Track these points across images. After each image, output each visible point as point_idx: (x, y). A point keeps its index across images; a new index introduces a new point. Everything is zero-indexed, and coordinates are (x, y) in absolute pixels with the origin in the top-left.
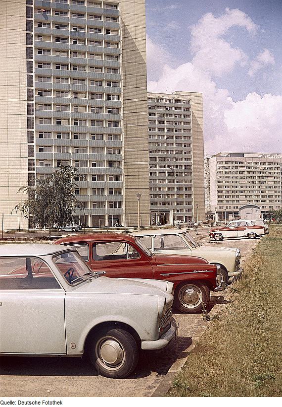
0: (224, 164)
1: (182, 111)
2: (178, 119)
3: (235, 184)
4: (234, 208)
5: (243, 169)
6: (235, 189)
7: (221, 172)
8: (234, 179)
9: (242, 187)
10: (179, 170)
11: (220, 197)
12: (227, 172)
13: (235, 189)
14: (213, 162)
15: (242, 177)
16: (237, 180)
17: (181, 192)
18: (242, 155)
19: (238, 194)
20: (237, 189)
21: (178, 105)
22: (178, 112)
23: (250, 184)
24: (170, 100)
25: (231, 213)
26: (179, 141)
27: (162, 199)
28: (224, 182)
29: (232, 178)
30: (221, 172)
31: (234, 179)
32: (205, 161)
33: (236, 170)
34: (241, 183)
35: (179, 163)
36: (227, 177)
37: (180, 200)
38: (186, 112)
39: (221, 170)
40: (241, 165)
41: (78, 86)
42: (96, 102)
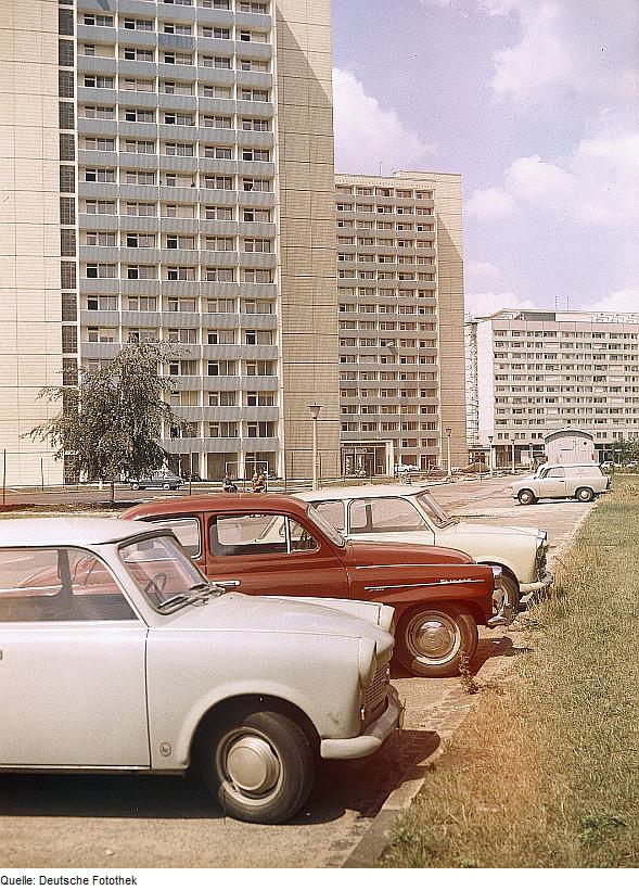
0: (509, 337)
1: (415, 217)
2: (406, 233)
3: (534, 383)
4: (534, 436)
5: (554, 349)
6: (534, 394)
7: (503, 355)
8: (534, 372)
9: (551, 389)
10: (408, 350)
11: (502, 411)
12: (518, 400)
13: (534, 394)
14: (485, 330)
15: (550, 367)
16: (540, 372)
17: (411, 400)
18: (552, 316)
19: (544, 404)
20: (540, 394)
21: (404, 201)
22: (405, 217)
23: (569, 383)
24: (387, 192)
25: (527, 447)
26: (406, 284)
27: (369, 418)
28: (510, 355)
29: (529, 368)
30: (503, 355)
31: (534, 372)
32: (468, 330)
33: (539, 350)
34: (549, 381)
35: (406, 334)
36: (518, 344)
37: (409, 417)
38: (424, 218)
39: (503, 350)
40: (548, 339)
41: (179, 161)
42: (217, 195)
